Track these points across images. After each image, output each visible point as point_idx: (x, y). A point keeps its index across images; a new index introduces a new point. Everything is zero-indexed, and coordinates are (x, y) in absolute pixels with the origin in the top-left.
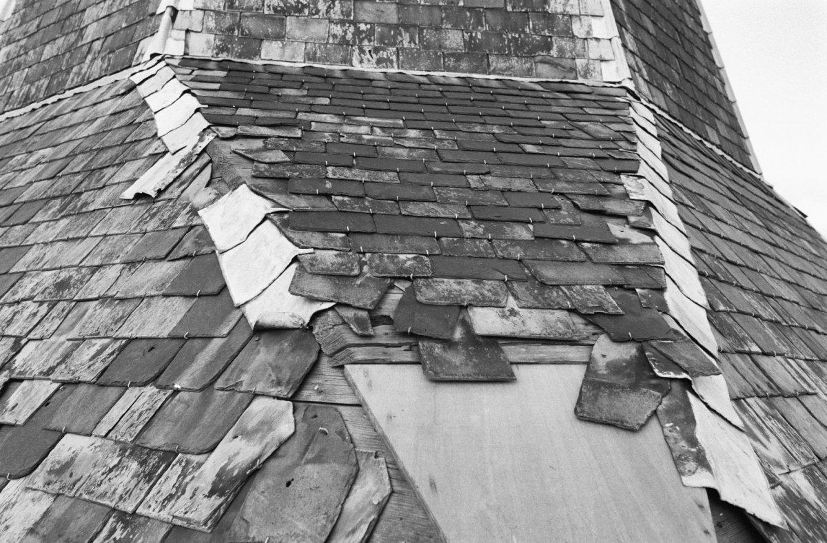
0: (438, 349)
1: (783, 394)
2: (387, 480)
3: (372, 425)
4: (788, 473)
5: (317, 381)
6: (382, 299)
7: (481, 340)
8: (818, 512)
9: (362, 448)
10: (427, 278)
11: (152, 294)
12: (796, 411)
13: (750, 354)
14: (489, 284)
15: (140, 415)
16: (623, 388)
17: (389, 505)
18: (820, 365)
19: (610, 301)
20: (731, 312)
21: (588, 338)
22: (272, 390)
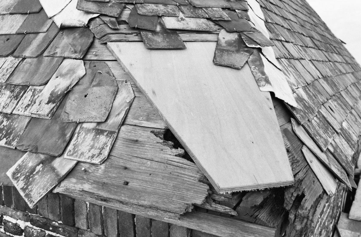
0: (150, 35)
1: (294, 59)
2: (132, 92)
3: (123, 69)
4: (297, 88)
5: (94, 51)
6: (121, 13)
7: (169, 31)
8: (308, 104)
9: (119, 79)
10: (142, 3)
11: (4, 13)
12: (297, 64)
13: (281, 41)
14: (170, 7)
15: (7, 70)
16: (233, 52)
17: (134, 102)
18: (306, 48)
19: (225, 15)
20: (273, 23)
21: (216, 31)
22: (72, 55)
